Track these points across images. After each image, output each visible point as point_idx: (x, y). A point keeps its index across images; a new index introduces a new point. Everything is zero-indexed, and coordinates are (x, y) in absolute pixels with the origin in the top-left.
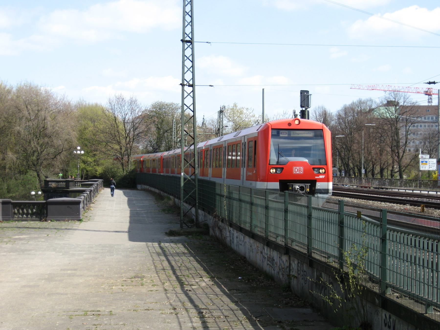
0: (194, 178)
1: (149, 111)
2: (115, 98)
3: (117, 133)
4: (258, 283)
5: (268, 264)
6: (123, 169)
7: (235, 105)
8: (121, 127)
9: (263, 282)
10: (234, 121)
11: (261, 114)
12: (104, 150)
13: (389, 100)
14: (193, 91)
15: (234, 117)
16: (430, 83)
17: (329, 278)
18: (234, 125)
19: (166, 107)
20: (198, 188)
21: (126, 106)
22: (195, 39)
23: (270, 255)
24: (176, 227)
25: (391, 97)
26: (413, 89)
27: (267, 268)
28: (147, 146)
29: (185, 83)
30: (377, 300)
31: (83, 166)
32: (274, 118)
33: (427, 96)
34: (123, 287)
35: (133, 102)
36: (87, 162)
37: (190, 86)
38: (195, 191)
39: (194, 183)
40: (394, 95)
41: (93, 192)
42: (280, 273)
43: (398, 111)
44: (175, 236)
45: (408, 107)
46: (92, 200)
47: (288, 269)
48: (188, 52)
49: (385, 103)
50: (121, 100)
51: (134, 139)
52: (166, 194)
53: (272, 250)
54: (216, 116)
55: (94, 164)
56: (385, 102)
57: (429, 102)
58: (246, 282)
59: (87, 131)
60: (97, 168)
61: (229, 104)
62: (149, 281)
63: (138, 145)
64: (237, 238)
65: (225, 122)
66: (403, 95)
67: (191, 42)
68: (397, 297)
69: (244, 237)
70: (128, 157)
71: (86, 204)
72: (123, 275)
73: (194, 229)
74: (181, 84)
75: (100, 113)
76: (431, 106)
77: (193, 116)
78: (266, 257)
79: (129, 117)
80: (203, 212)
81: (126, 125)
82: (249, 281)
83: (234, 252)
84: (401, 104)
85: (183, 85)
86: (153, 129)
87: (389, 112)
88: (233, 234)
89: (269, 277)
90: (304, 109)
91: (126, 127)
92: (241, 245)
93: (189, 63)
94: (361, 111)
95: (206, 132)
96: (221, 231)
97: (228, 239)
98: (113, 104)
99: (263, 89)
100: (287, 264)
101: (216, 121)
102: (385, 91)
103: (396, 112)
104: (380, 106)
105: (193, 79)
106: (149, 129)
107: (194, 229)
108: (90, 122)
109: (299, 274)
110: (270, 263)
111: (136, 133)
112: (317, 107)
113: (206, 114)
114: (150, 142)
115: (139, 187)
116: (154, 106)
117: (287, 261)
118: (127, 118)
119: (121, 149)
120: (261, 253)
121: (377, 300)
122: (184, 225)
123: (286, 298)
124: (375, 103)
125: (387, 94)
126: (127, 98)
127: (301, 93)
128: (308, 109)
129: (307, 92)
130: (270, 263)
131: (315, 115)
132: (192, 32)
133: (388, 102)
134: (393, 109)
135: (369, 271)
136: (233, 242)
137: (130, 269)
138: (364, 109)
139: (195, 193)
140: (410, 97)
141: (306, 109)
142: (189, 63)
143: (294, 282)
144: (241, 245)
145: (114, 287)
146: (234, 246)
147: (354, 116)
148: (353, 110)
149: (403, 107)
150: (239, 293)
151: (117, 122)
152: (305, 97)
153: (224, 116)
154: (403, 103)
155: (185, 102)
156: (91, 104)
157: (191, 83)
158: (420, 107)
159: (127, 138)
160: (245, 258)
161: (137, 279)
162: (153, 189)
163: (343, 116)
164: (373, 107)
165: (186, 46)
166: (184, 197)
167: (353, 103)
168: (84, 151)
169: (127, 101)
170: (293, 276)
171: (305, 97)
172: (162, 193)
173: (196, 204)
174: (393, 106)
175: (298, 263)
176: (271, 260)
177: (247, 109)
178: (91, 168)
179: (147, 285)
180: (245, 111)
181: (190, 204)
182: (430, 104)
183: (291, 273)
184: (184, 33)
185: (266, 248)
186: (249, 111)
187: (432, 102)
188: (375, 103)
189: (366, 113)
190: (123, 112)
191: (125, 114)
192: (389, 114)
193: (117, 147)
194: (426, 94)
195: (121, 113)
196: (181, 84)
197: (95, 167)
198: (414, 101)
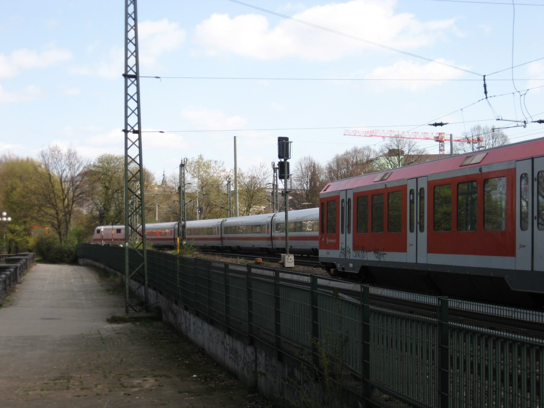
0: (142, 248)
1: (95, 166)
2: (49, 150)
3: (52, 194)
4: (218, 382)
5: (230, 358)
6: (61, 240)
7: (201, 157)
8: (57, 186)
9: (224, 381)
10: (201, 178)
11: (233, 168)
12: (35, 215)
13: (391, 149)
14: (140, 139)
15: (199, 172)
16: (436, 125)
17: (303, 375)
18: (200, 183)
19: (115, 161)
20: (147, 262)
21: (62, 161)
22: (141, 74)
23: (233, 346)
24: (120, 313)
25: (392, 144)
26: (420, 134)
27: (229, 363)
28: (92, 210)
29: (129, 128)
30: (360, 404)
31: (10, 236)
32: (248, 172)
33: (438, 143)
34: (42, 393)
35: (71, 155)
36: (16, 231)
37: (135, 132)
38: (144, 265)
39: (141, 255)
40: (397, 141)
41: (20, 269)
42: (245, 369)
43: (403, 161)
44: (118, 323)
45: (413, 156)
46: (19, 279)
47: (253, 365)
48: (132, 90)
49: (386, 152)
50: (56, 153)
51: (73, 202)
52: (112, 270)
53: (234, 339)
54: (177, 171)
55: (24, 233)
56: (386, 151)
57: (440, 150)
58: (203, 381)
59: (15, 192)
60: (28, 238)
61: (192, 156)
62: (77, 383)
63: (81, 209)
64: (194, 324)
65: (188, 177)
66: (408, 141)
67: (136, 77)
68: (386, 400)
69: (202, 323)
70: (67, 224)
71: (10, 285)
72: (45, 376)
73: (143, 314)
74: (124, 130)
75: (31, 169)
76: (444, 155)
77: (140, 171)
78: (228, 348)
79: (67, 173)
80: (154, 292)
81: (63, 184)
82: (206, 380)
83: (190, 342)
84: (406, 152)
85: (126, 131)
86: (100, 188)
87: (392, 163)
88: (189, 320)
89: (232, 374)
90: (283, 160)
91: (63, 187)
92: (199, 333)
93: (133, 104)
94: (357, 162)
95: (165, 192)
96: (175, 316)
97: (184, 326)
98: (47, 158)
99: (235, 137)
100: (253, 358)
101: (178, 177)
102: (383, 137)
103: (399, 162)
104: (381, 156)
105: (139, 123)
106: (93, 188)
107: (143, 314)
108: (18, 181)
109: (267, 370)
110: (232, 357)
111: (76, 194)
112: (303, 158)
113: (161, 166)
114: (96, 204)
115: (81, 261)
116: (102, 160)
117: (252, 353)
118: (64, 175)
119: (57, 214)
120: (223, 343)
121: (360, 404)
122: (130, 309)
123: (251, 402)
124: (374, 152)
125: (387, 141)
126: (64, 151)
127: (279, 140)
128: (288, 161)
129: (287, 139)
130: (232, 357)
131: (300, 168)
132: (137, 64)
133: (390, 150)
134: (395, 159)
135: (350, 366)
136: (190, 330)
137: (55, 367)
138: (360, 161)
139: (143, 267)
140: (417, 144)
141: (285, 160)
142: (133, 104)
143: (262, 382)
144: (199, 333)
145: (30, 393)
146: (191, 335)
147: (348, 168)
148: (347, 161)
149: (408, 156)
150: (192, 396)
151: (52, 181)
152: (284, 146)
153: (186, 172)
154: (407, 151)
155: (130, 153)
156: (20, 158)
157: (136, 128)
158: (428, 156)
159: (64, 200)
160: (203, 349)
161: (61, 381)
162: (97, 264)
163: (336, 168)
164: (372, 157)
165: (129, 82)
166: (130, 273)
167: (347, 152)
168: (12, 218)
169: (64, 154)
170: (260, 372)
171: (284, 146)
172: (107, 268)
173: (144, 282)
174: (396, 155)
175: (266, 356)
176: (234, 352)
177: (216, 162)
178: (20, 239)
179: (74, 389)
180: (213, 165)
181: (139, 282)
182: (441, 153)
183: (258, 369)
184: (127, 66)
185: (227, 337)
186: (218, 164)
187: (444, 150)
188: (374, 152)
189: (363, 164)
190: (59, 168)
191: (61, 170)
192: (391, 165)
193: (53, 212)
194: (437, 141)
195: (56, 168)
196: (124, 130)
197: (26, 237)
198: (421, 148)
